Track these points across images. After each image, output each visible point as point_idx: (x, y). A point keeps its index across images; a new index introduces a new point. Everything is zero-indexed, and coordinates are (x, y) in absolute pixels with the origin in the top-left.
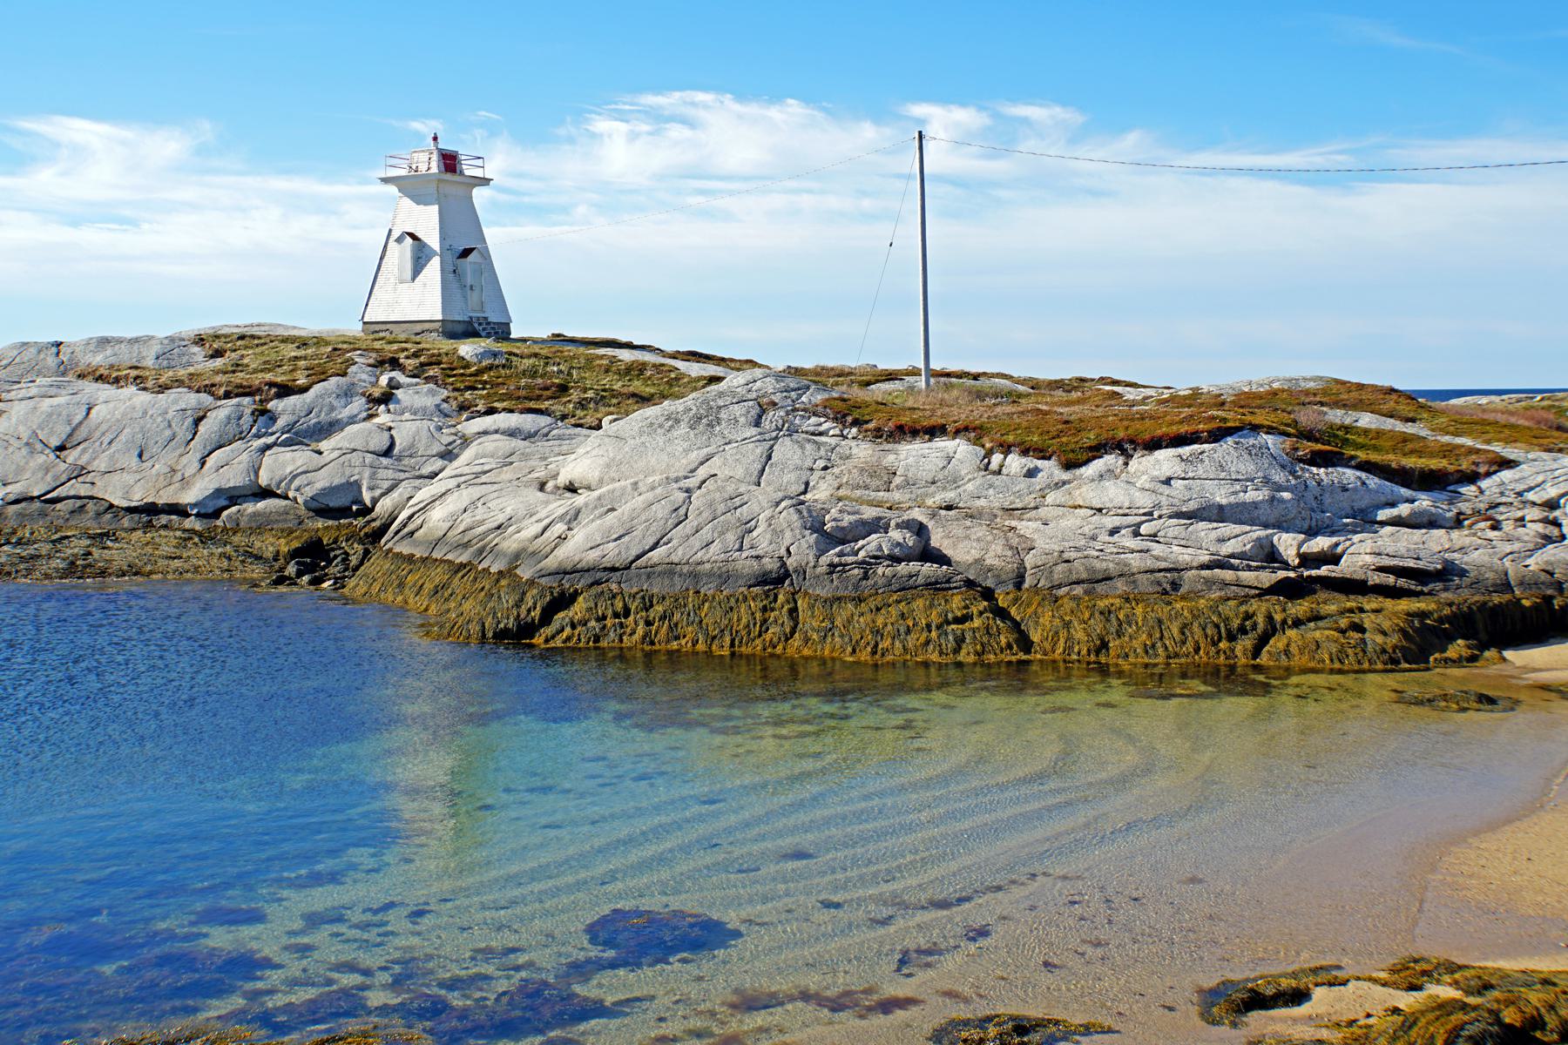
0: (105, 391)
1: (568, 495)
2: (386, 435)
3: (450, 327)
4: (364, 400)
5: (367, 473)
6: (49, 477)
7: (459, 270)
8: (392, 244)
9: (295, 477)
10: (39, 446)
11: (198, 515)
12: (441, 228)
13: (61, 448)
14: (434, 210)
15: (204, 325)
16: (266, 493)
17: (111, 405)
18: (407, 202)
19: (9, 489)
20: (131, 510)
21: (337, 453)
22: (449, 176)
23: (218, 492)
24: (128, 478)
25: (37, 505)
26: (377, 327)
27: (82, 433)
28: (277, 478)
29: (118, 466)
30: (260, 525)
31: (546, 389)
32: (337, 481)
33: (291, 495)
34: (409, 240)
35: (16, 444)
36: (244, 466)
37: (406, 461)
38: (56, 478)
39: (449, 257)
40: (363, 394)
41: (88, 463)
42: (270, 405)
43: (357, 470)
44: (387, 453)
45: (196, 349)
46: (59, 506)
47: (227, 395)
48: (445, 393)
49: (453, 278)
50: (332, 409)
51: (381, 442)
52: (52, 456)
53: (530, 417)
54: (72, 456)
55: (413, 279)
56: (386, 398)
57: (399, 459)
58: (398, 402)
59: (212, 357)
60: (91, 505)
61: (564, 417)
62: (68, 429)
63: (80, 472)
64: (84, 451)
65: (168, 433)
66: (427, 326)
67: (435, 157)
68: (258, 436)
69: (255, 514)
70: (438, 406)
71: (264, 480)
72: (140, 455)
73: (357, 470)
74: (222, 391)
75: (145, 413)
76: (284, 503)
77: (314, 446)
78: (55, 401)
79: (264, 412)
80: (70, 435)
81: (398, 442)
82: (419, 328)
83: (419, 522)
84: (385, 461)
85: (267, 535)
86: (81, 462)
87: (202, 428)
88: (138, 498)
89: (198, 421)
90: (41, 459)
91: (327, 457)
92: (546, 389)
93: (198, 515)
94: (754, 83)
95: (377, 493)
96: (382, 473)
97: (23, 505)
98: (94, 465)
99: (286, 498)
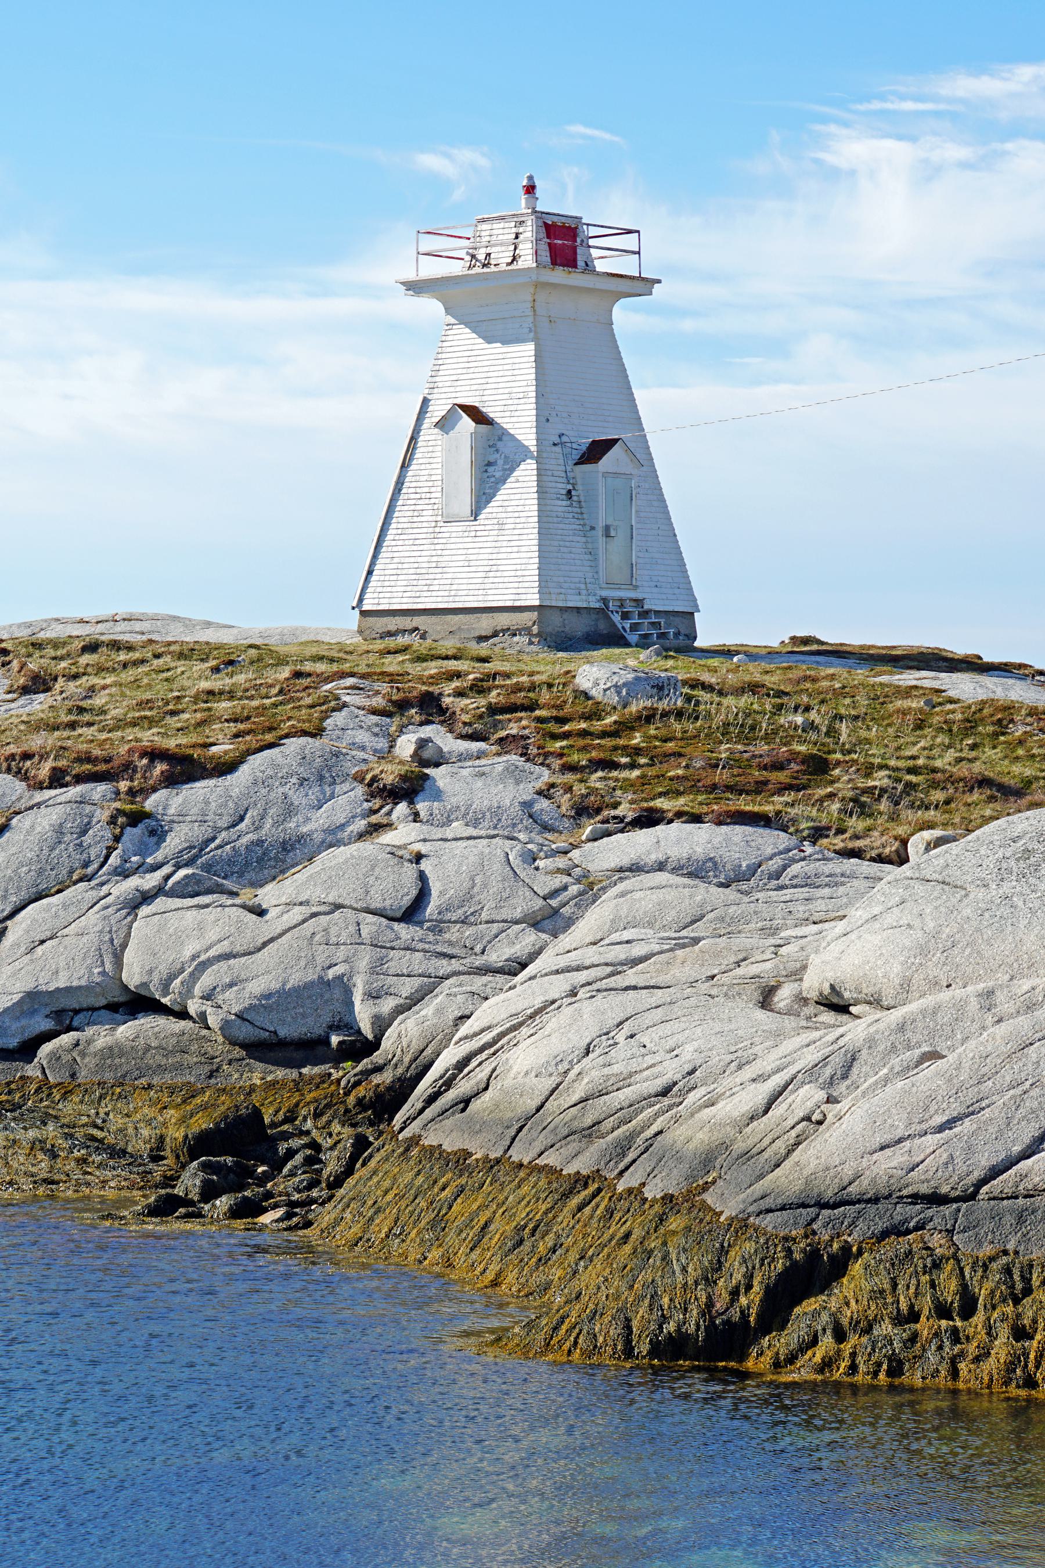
1: (828, 1017)
2: (409, 871)
3: (556, 622)
8: (429, 434)
9: (204, 966)
16: (138, 1004)
21: (297, 914)
22: (560, 276)
23: (33, 999)
28: (163, 970)
30: (122, 1080)
32: (296, 979)
34: (467, 423)
37: (453, 933)
39: (557, 460)
40: (359, 778)
43: (341, 953)
47: (57, 779)
48: (545, 776)
49: (566, 507)
50: (289, 810)
53: (739, 832)
55: (475, 514)
56: (410, 788)
57: (437, 928)
59: (25, 690)
66: (504, 620)
67: (528, 232)
68: (123, 873)
70: (527, 805)
71: (132, 976)
73: (341, 953)
74: (44, 771)
79: (136, 818)
82: (485, 624)
84: (405, 932)
91: (275, 921)
95: (387, 1005)
96: (399, 961)
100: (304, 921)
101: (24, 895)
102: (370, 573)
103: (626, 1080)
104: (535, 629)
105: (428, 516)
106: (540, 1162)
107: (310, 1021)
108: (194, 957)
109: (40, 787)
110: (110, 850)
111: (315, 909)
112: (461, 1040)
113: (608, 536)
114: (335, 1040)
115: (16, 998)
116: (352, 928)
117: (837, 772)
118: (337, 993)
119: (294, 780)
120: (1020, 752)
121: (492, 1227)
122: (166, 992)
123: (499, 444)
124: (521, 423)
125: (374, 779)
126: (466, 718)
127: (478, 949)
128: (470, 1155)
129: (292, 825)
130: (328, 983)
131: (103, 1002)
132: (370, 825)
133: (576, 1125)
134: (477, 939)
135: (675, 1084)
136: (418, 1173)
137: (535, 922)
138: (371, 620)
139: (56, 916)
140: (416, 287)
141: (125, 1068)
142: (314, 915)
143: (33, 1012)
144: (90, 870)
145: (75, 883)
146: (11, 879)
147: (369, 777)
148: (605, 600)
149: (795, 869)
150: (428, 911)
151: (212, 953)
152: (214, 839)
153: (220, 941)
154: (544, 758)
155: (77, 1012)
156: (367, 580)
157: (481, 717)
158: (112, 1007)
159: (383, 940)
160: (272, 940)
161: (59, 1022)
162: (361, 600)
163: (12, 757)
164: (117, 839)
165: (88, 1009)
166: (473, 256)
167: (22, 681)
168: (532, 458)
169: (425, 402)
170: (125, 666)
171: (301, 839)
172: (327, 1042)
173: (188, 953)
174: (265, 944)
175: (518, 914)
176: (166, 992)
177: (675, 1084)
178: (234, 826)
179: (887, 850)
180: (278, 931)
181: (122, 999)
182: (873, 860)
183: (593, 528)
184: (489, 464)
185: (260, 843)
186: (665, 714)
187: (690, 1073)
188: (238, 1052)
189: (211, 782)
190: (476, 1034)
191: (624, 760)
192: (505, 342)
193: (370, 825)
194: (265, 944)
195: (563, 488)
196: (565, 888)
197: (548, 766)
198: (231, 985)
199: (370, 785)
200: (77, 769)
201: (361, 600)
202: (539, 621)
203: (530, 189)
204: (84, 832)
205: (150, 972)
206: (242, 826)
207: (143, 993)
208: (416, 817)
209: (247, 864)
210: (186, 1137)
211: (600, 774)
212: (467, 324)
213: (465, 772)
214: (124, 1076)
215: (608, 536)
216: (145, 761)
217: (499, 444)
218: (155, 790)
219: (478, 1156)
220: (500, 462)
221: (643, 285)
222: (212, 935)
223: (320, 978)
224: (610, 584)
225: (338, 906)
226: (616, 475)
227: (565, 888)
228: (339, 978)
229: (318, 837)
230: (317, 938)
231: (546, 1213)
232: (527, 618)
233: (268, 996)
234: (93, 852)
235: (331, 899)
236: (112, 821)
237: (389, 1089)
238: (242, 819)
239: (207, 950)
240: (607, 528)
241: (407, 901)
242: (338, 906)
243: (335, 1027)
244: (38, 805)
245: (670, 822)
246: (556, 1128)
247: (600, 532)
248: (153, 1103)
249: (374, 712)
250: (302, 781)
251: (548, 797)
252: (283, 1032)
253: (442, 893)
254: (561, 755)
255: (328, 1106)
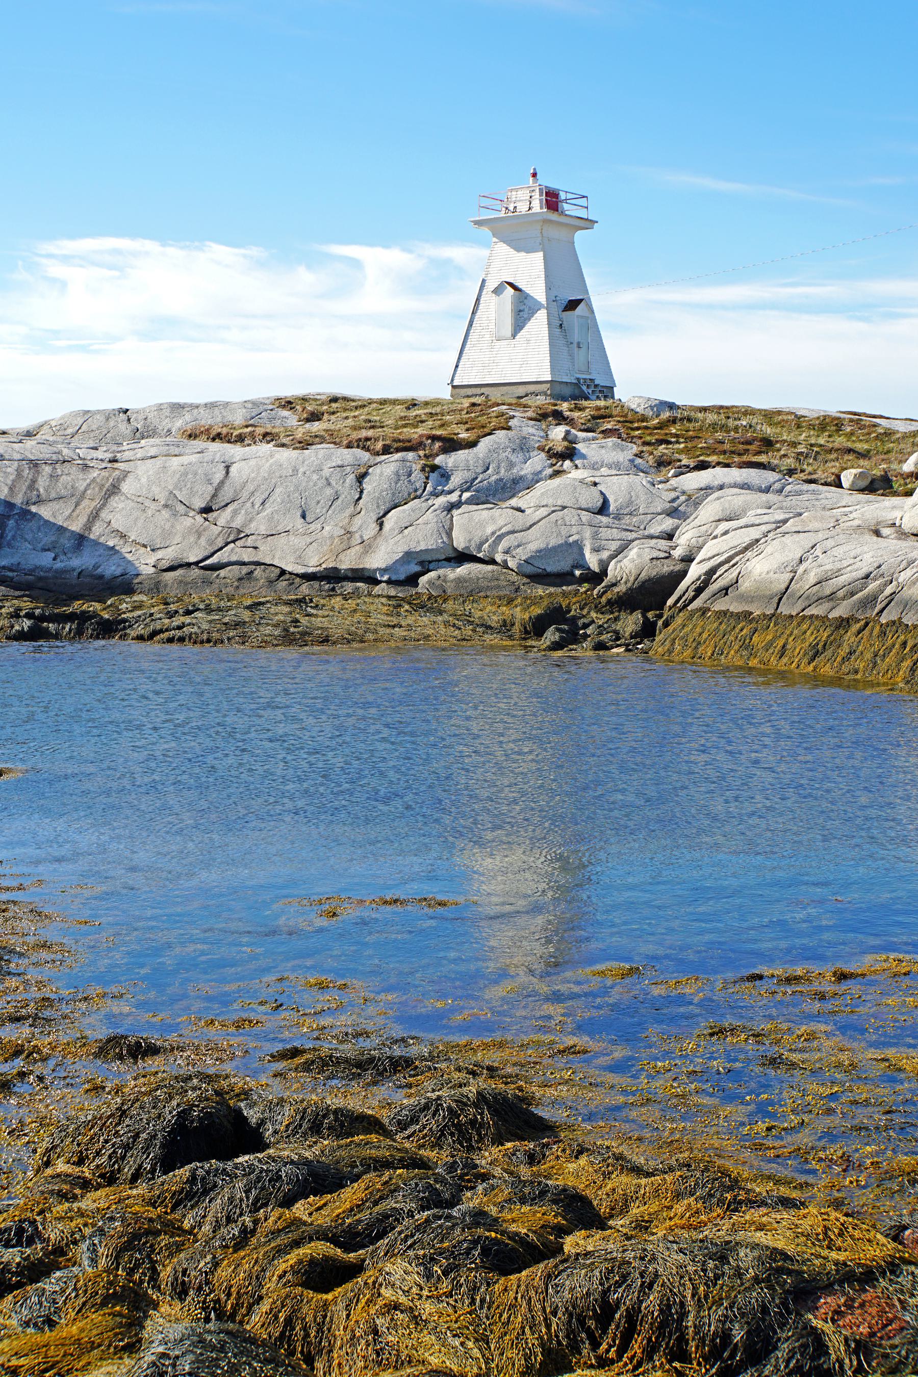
0: (235, 451)
3: (558, 389)
4: (543, 455)
5: (588, 533)
6: (203, 541)
7: (565, 325)
8: (487, 296)
9: (500, 538)
10: (181, 509)
11: (389, 582)
12: (547, 276)
13: (207, 510)
14: (540, 255)
15: (289, 392)
16: (462, 557)
17: (252, 462)
18: (503, 249)
19: (160, 554)
20: (308, 577)
21: (543, 512)
22: (554, 216)
23: (408, 556)
24: (297, 541)
25: (195, 572)
26: (469, 392)
27: (227, 494)
28: (477, 540)
29: (280, 528)
30: (471, 592)
31: (748, 443)
32: (553, 542)
33: (499, 558)
34: (510, 291)
35: (153, 506)
36: (432, 526)
37: (627, 520)
38: (211, 542)
39: (556, 310)
40: (541, 448)
41: (245, 525)
42: (438, 460)
43: (574, 530)
44: (603, 509)
45: (285, 413)
46: (222, 573)
47: (386, 450)
48: (635, 449)
49: (559, 331)
50: (511, 465)
51: (592, 499)
52: (199, 519)
53: (753, 472)
54: (223, 517)
55: (514, 336)
56: (569, 453)
57: (618, 517)
58: (584, 457)
59: (308, 420)
60: (258, 572)
61: (791, 472)
62: (210, 489)
63: (237, 536)
64: (235, 512)
65: (329, 492)
66: (531, 388)
67: (536, 195)
68: (436, 495)
69: (459, 580)
70: (632, 461)
71: (460, 542)
72: (304, 516)
73: (574, 530)
74: (379, 446)
75: (295, 471)
76: (490, 567)
77: (514, 502)
78: (185, 459)
79: (434, 468)
80: (214, 496)
81: (611, 499)
82: (521, 390)
83: (733, 574)
84: (604, 519)
85: (483, 603)
86: (237, 523)
87: (368, 484)
88: (313, 564)
89: (360, 478)
90: (188, 522)
91: (533, 515)
92: (748, 443)
93: (389, 582)
94: (184, 227)
95: (605, 555)
96: (605, 533)
97: (180, 572)
98: (252, 528)
99: (493, 562)
100: (549, 515)
101: (388, 505)
102: (457, 366)
103: (838, 573)
104: (549, 392)
105: (487, 337)
106: (807, 612)
107: (562, 563)
108: (493, 533)
109: (377, 454)
110: (426, 484)
111: (553, 509)
112: (701, 562)
113: (579, 347)
114: (577, 573)
115: (401, 555)
116: (576, 518)
117: (778, 445)
118: (575, 550)
119: (509, 450)
120: (854, 438)
121: (788, 647)
122: (479, 550)
123: (525, 301)
124: (538, 292)
125: (550, 449)
126: (582, 421)
127: (642, 527)
128: (751, 613)
129: (515, 471)
130: (570, 544)
131: (444, 557)
132: (554, 471)
133: (820, 594)
134: (641, 522)
135: (871, 573)
136: (721, 623)
137: (673, 512)
138: (457, 390)
139: (409, 515)
140: (477, 223)
141: (471, 588)
142: (553, 512)
143: (409, 562)
144: (418, 493)
145: (413, 499)
146: (379, 498)
147: (547, 448)
148: (578, 379)
149: (788, 488)
150: (611, 509)
151: (503, 530)
152: (477, 478)
153: (506, 525)
154: (631, 440)
155: (430, 562)
156: (455, 370)
157: (589, 420)
158: (448, 560)
159: (593, 523)
160: (534, 524)
161: (423, 567)
162: (452, 380)
163: (360, 440)
164: (427, 478)
165: (436, 561)
166: (507, 208)
167: (305, 416)
168: (544, 307)
169: (484, 281)
170: (356, 408)
171: (521, 478)
172: (573, 575)
173: (489, 530)
174: (531, 526)
175: (659, 510)
176: (480, 551)
177: (871, 573)
178: (485, 472)
179: (829, 480)
180: (537, 519)
181: (453, 556)
182: (822, 484)
183: (572, 343)
184: (520, 311)
185: (501, 480)
186: (682, 419)
187: (879, 567)
188: (525, 580)
189: (467, 451)
190: (710, 559)
191: (673, 440)
192: (528, 251)
193: (554, 471)
194: (531, 526)
195: (558, 323)
196: (678, 498)
197: (635, 443)
198: (519, 546)
199: (548, 452)
200: (396, 445)
201: (452, 380)
202: (551, 388)
203: (534, 175)
204: (410, 475)
205: (470, 541)
206: (489, 472)
207: (466, 552)
208: (577, 467)
209: (496, 490)
210: (530, 618)
211: (663, 446)
212: (504, 242)
213: (593, 446)
214: (471, 591)
215: (579, 347)
216: (429, 441)
217: (525, 301)
218: (438, 455)
219: (758, 613)
220: (526, 310)
221: (589, 223)
222: (501, 522)
223: (566, 542)
224: (580, 372)
225: (564, 508)
226: (582, 317)
227: (678, 498)
228: (576, 542)
229: (530, 477)
230: (559, 522)
231: (828, 637)
232: (544, 387)
233: (540, 551)
234: (418, 485)
235: (559, 503)
236: (423, 470)
237: (625, 594)
238: (488, 469)
239: (500, 529)
240: (579, 344)
241: (599, 504)
242: (564, 508)
243: (577, 566)
244: (380, 463)
245: (714, 467)
246: (808, 597)
247: (575, 345)
248: (493, 604)
249: (531, 419)
250: (514, 450)
251: (641, 457)
252: (549, 570)
253: (616, 501)
254: (641, 438)
255: (586, 604)
